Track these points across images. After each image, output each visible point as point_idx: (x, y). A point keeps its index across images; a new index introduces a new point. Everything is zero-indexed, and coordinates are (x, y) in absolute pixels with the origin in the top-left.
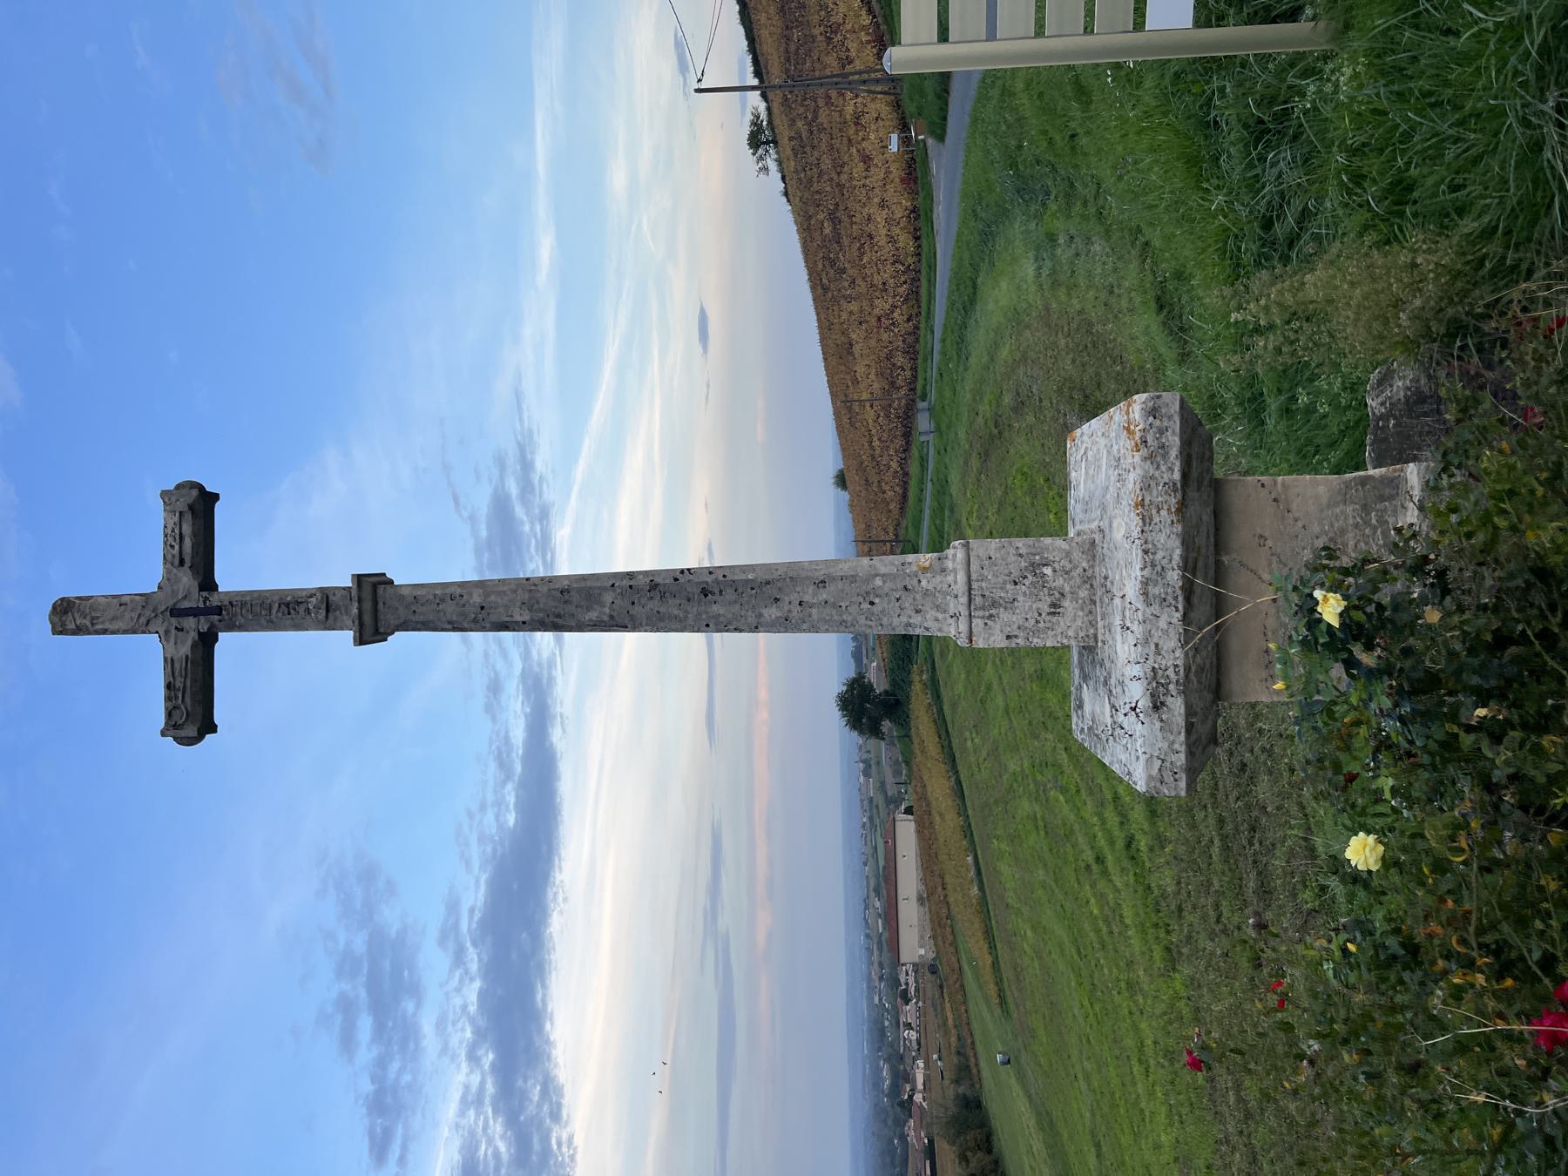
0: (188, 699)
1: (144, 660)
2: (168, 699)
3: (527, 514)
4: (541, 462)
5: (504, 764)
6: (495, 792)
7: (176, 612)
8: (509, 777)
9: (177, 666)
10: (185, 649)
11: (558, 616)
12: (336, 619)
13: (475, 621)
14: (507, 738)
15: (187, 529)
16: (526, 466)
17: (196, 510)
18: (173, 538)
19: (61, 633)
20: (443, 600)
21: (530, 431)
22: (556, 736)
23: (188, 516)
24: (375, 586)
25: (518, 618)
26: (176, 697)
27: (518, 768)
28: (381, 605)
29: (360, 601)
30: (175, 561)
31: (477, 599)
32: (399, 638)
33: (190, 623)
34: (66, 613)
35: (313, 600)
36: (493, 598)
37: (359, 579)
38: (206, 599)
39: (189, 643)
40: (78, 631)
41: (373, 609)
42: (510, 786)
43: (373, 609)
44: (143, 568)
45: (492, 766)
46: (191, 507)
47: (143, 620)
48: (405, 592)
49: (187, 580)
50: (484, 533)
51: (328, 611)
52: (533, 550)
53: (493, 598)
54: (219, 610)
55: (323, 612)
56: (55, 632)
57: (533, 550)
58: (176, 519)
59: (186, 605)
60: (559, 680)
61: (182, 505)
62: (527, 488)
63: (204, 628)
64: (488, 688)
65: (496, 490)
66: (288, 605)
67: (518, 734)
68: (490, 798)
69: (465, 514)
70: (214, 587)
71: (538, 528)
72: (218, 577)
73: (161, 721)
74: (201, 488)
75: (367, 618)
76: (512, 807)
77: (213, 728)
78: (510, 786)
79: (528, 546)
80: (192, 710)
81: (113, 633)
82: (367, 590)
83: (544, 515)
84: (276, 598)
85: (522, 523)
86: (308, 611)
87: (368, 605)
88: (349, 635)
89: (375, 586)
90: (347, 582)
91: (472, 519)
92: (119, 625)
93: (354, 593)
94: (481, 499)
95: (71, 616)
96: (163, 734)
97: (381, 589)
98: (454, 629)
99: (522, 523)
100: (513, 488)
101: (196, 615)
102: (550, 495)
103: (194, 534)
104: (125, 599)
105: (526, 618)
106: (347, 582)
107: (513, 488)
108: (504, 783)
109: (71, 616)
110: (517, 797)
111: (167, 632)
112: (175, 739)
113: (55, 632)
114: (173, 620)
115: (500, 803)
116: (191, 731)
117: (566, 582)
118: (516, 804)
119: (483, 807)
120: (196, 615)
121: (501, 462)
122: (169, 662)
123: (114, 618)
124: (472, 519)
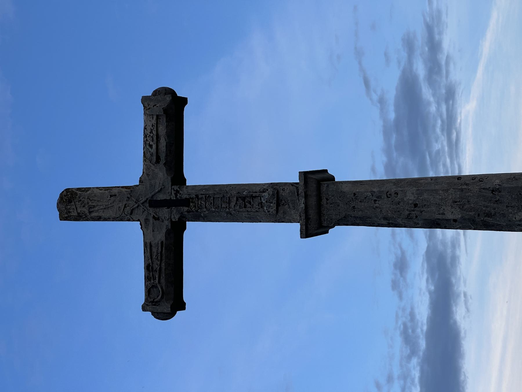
0: (163, 281)
1: (127, 242)
2: (147, 278)
3: (434, 95)
4: (449, 41)
5: (408, 339)
6: (401, 366)
7: (154, 203)
8: (413, 353)
9: (154, 250)
10: (161, 236)
11: (489, 215)
12: (284, 213)
13: (409, 217)
14: (412, 315)
15: (162, 130)
16: (434, 46)
17: (167, 113)
18: (151, 138)
19: (66, 219)
20: (379, 197)
21: (439, 12)
22: (460, 314)
23: (163, 120)
24: (319, 183)
25: (450, 216)
26: (154, 279)
27: (423, 344)
28: (324, 201)
29: (306, 196)
30: (152, 158)
31: (410, 196)
32: (337, 231)
33: (164, 212)
34: (70, 202)
35: (266, 194)
36: (425, 196)
37: (305, 175)
38: (177, 192)
39: (164, 231)
40: (79, 218)
41: (317, 203)
42: (415, 361)
43: (317, 203)
44: (126, 166)
45: (399, 341)
46: (165, 111)
47: (128, 209)
48: (346, 189)
49: (162, 175)
50: (392, 116)
51: (278, 205)
52: (438, 130)
53: (425, 196)
54: (186, 202)
55: (274, 205)
56: (62, 218)
57: (438, 130)
58: (154, 121)
59: (161, 197)
60: (463, 259)
61: (158, 110)
62: (435, 68)
63: (176, 217)
64: (395, 265)
65: (404, 72)
66: (244, 199)
67: (423, 312)
68: (396, 372)
69: (375, 97)
70: (184, 181)
71: (444, 108)
72: (187, 173)
73: (141, 298)
74: (172, 93)
75: (312, 213)
76: (417, 380)
77: (182, 306)
78: (415, 361)
79: (434, 126)
80: (165, 293)
81: (105, 220)
82: (313, 186)
83: (450, 95)
84: (234, 193)
85: (429, 104)
86: (261, 204)
87: (313, 201)
88: (296, 227)
89: (319, 183)
90: (296, 179)
91: (382, 101)
92: (110, 213)
93: (301, 190)
94: (389, 84)
95: (76, 205)
96: (144, 309)
97: (325, 184)
98: (389, 225)
99: (429, 104)
100: (420, 69)
101: (167, 205)
102: (456, 74)
103: (168, 135)
104: (115, 191)
105: (458, 216)
106: (296, 179)
107: (420, 69)
108: (409, 358)
109: (76, 205)
110: (422, 371)
111: (146, 220)
112: (153, 314)
113: (62, 218)
114: (151, 210)
115: (405, 377)
116: (166, 308)
117: (497, 182)
118: (421, 378)
119: (390, 379)
120: (167, 205)
121: (409, 44)
122: (148, 247)
123: (106, 208)
124: (382, 101)
